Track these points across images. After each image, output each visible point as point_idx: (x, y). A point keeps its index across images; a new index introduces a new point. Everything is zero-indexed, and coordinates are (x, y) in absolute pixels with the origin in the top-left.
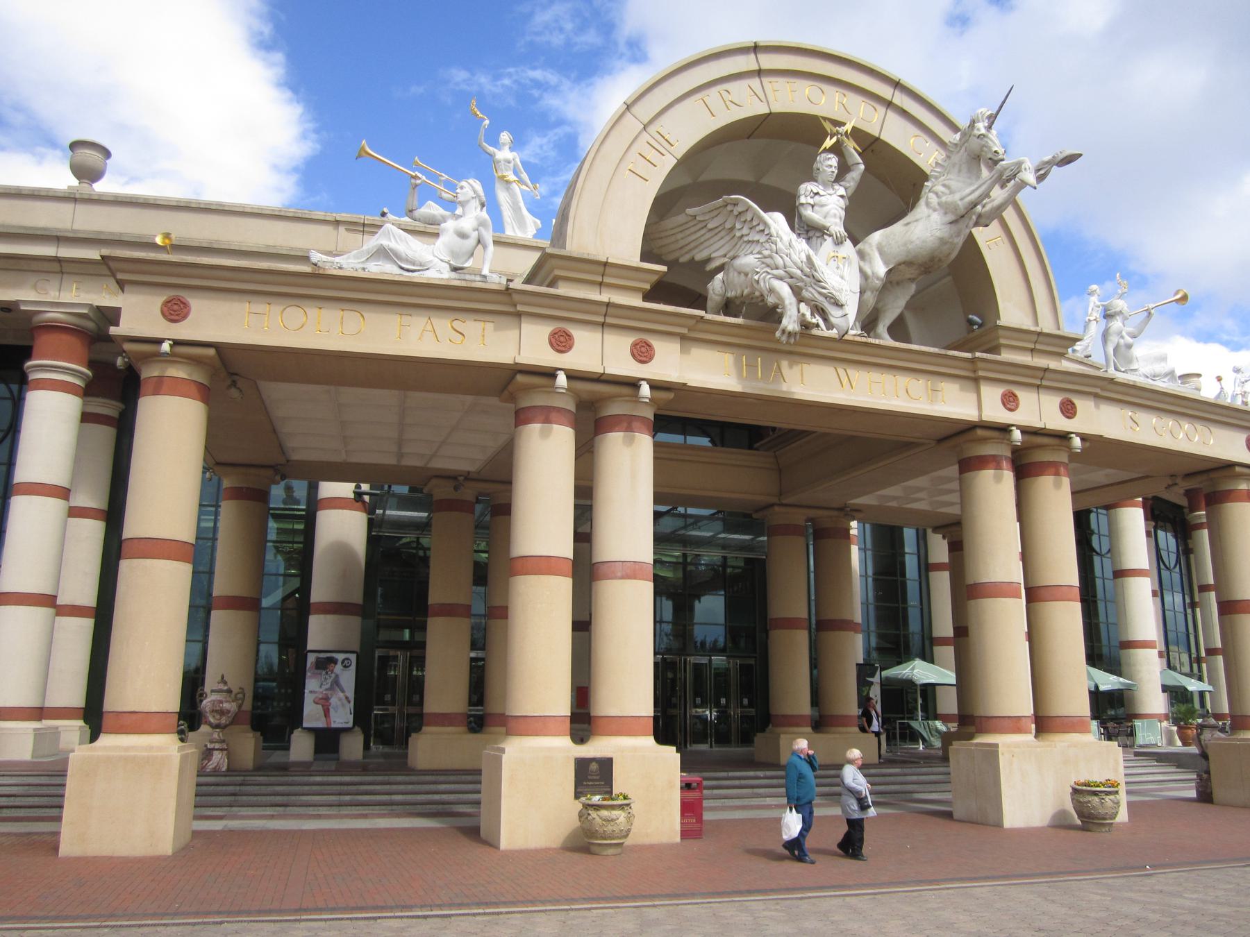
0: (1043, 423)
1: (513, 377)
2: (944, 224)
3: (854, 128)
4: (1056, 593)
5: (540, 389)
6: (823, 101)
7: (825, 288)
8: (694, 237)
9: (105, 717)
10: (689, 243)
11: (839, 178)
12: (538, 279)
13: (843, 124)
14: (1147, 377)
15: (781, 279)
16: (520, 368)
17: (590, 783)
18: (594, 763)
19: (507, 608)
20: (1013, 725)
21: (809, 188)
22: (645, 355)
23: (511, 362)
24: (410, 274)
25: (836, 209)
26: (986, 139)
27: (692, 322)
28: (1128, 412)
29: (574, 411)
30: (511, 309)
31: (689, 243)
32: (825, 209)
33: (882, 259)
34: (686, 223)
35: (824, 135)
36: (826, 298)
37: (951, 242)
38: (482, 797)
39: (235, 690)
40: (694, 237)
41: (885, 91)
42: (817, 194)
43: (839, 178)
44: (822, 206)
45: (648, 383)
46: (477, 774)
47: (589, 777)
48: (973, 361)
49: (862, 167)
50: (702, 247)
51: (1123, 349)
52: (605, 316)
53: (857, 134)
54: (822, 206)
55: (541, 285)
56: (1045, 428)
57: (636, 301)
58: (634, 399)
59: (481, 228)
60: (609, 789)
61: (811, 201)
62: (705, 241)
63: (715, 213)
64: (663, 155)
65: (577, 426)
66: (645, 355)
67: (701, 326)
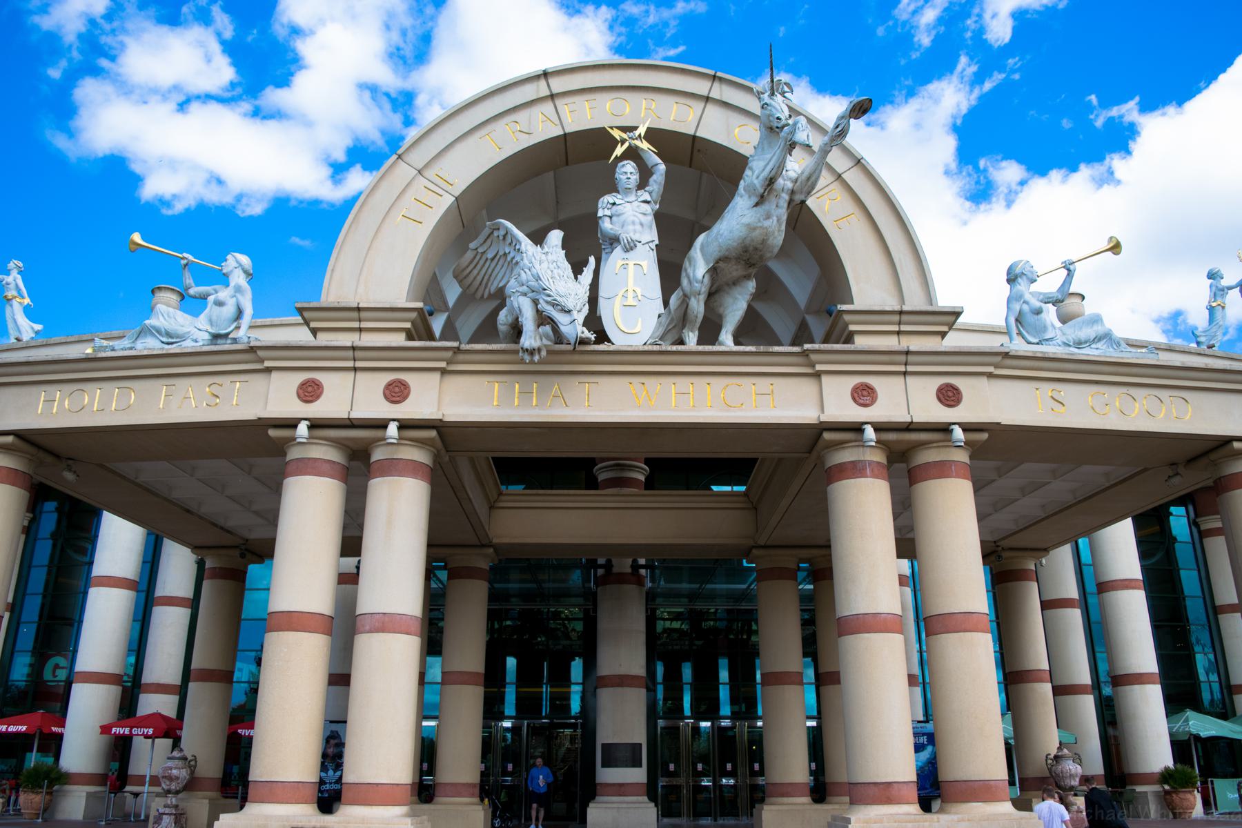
0: (441, 413)
1: (821, 434)
2: (748, 209)
3: (649, 130)
4: (960, 623)
5: (847, 445)
6: (628, 111)
7: (549, 296)
10: (483, 278)
11: (642, 185)
12: (834, 337)
13: (636, 128)
14: (1069, 346)
15: (525, 294)
19: (838, 673)
20: (884, 793)
21: (606, 201)
22: (953, 398)
23: (814, 421)
24: (170, 346)
25: (634, 216)
26: (769, 108)
27: (449, 354)
28: (1047, 388)
29: (968, 463)
30: (809, 370)
31: (483, 278)
32: (622, 218)
33: (704, 259)
34: (475, 257)
35: (614, 143)
36: (553, 306)
37: (761, 227)
39: (190, 758)
42: (614, 204)
43: (642, 185)
44: (618, 215)
45: (872, 427)
49: (662, 167)
50: (492, 279)
51: (1030, 318)
53: (653, 135)
54: (618, 215)
55: (837, 343)
56: (912, 422)
57: (399, 340)
58: (861, 443)
59: (238, 295)
61: (608, 213)
62: (492, 272)
63: (489, 241)
64: (441, 196)
65: (891, 478)
66: (953, 398)
67: (461, 357)
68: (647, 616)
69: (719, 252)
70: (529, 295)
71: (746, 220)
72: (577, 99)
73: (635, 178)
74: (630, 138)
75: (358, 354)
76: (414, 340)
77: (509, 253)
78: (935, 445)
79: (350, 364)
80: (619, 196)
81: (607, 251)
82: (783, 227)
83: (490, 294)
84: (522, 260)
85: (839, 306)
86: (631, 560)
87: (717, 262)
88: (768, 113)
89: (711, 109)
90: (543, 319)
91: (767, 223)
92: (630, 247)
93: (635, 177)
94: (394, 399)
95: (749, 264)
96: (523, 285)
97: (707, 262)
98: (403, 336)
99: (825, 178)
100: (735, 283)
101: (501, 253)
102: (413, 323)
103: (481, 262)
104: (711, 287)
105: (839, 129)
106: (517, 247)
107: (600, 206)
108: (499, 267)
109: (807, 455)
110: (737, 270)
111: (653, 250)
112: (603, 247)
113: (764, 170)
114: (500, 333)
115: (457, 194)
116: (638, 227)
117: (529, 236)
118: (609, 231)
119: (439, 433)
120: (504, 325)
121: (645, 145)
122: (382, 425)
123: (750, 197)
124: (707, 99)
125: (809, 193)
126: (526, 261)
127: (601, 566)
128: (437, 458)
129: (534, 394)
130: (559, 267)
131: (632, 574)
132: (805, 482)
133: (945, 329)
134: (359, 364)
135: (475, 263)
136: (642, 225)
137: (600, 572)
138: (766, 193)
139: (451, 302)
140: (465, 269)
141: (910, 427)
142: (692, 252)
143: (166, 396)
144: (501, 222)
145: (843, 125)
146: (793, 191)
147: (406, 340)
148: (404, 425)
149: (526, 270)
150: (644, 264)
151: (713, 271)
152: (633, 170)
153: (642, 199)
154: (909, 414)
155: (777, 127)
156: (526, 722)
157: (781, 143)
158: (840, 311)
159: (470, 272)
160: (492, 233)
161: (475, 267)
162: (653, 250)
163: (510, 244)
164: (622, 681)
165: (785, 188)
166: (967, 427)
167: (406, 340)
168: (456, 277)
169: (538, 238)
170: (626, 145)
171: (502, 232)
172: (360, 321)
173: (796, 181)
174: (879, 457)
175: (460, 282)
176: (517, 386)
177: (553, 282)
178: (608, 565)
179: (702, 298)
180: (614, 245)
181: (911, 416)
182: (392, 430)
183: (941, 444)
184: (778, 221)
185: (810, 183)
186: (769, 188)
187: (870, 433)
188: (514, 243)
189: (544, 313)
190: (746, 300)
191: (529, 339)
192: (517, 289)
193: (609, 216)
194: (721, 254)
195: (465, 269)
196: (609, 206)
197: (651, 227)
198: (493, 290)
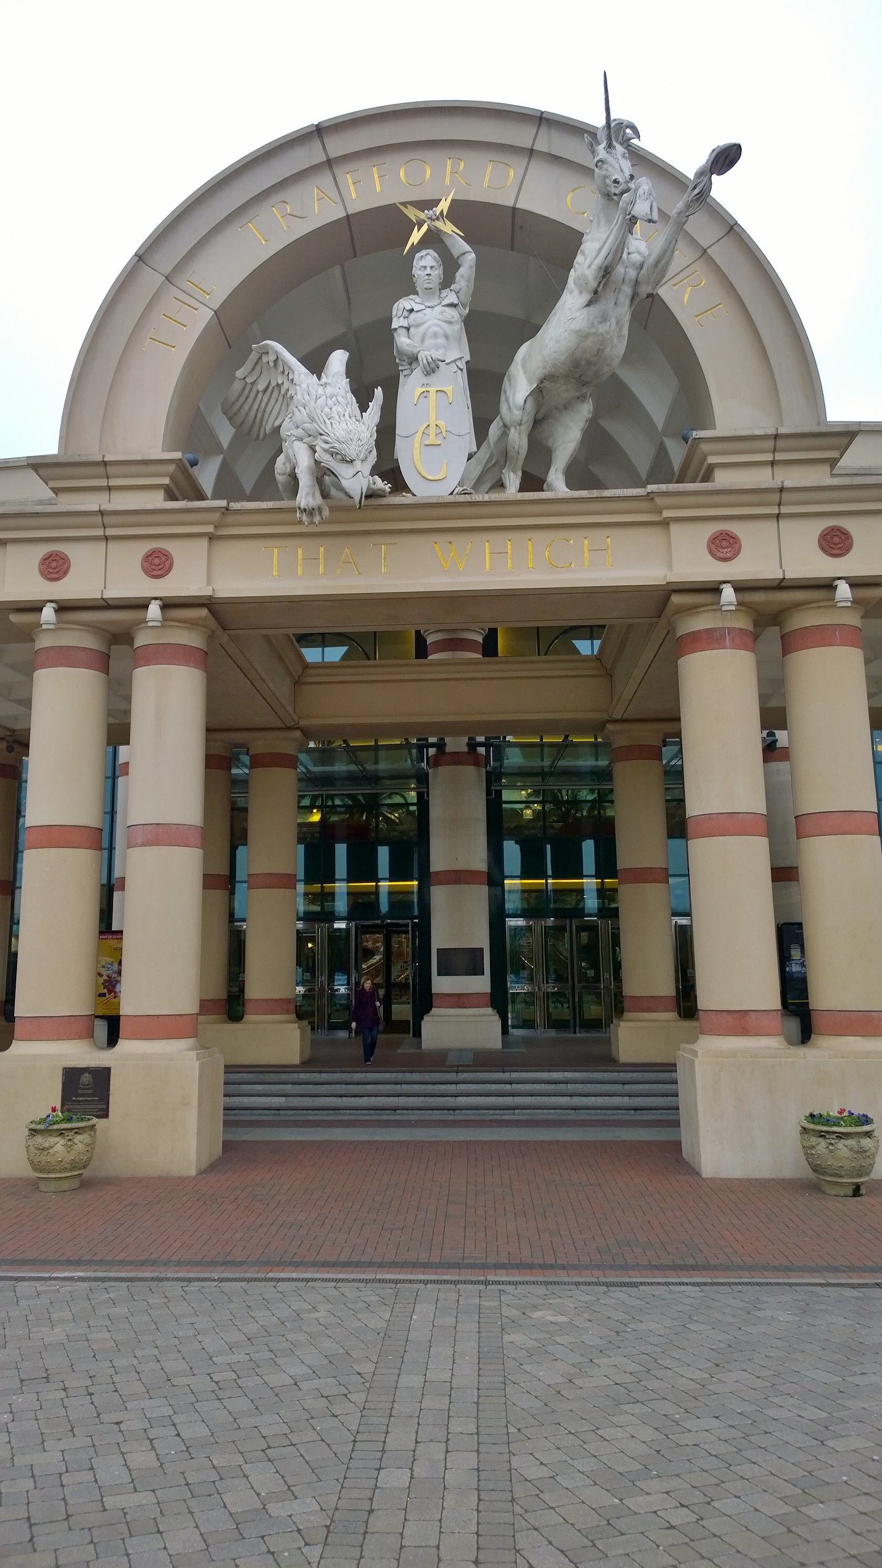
1: (667, 599)
5: (809, 606)
7: (327, 443)
8: (256, 406)
9: (434, 998)
10: (256, 415)
11: (447, 281)
13: (436, 202)
15: (300, 439)
16: (674, 588)
17: (81, 1099)
18: (86, 1074)
21: (401, 306)
22: (839, 546)
26: (605, 166)
27: (216, 516)
31: (256, 415)
32: (422, 329)
34: (244, 389)
35: (410, 226)
37: (595, 333)
38: (682, 1101)
40: (256, 406)
41: (522, 136)
42: (412, 311)
44: (418, 326)
46: (671, 1071)
47: (80, 1091)
48: (650, 497)
49: (471, 257)
52: (779, 505)
57: (157, 500)
60: (104, 1107)
64: (196, 309)
66: (839, 546)
67: (230, 519)
68: (488, 801)
69: (544, 368)
70: (306, 440)
71: (576, 325)
72: (362, 166)
73: (438, 273)
74: (429, 218)
75: (107, 520)
76: (177, 500)
77: (283, 383)
78: (814, 605)
79: (99, 532)
80: (418, 300)
81: (405, 373)
82: (625, 331)
83: (265, 434)
84: (296, 394)
85: (694, 433)
86: (467, 739)
87: (542, 382)
88: (604, 173)
89: (538, 170)
90: (322, 474)
91: (602, 328)
92: (431, 369)
93: (437, 272)
94: (155, 573)
95: (583, 383)
96: (298, 427)
97: (530, 381)
98: (161, 494)
99: (682, 257)
100: (567, 406)
101: (273, 384)
102: (172, 478)
103: (252, 395)
104: (537, 412)
105: (697, 191)
106: (290, 377)
107: (394, 313)
108: (273, 401)
109: (656, 620)
110: (567, 391)
111: (462, 370)
112: (400, 368)
113: (598, 255)
114: (279, 485)
115: (216, 307)
116: (441, 341)
117: (304, 361)
118: (406, 348)
119: (210, 610)
120: (283, 474)
121: (448, 228)
122: (142, 605)
123: (581, 293)
124: (531, 153)
125: (657, 283)
126: (299, 396)
127: (433, 745)
128: (211, 637)
129: (321, 561)
130: (339, 403)
131: (468, 753)
132: (658, 650)
133: (834, 454)
134: (110, 532)
135: (245, 395)
136: (446, 337)
137: (432, 751)
138: (601, 287)
139: (225, 444)
140: (234, 403)
141: (783, 584)
142: (512, 368)
143: (318, 200)
144: (268, 345)
145: (702, 185)
146: (637, 281)
147: (165, 500)
148: (168, 605)
149: (300, 408)
150: (449, 389)
151: (538, 393)
152: (433, 263)
153: (447, 301)
154: (781, 568)
155: (615, 194)
156: (354, 923)
157: (618, 217)
158: (695, 439)
159: (241, 407)
160: (260, 358)
161: (245, 401)
162: (462, 370)
163: (283, 372)
164: (458, 877)
165: (627, 277)
166: (855, 582)
167: (165, 500)
168: (225, 413)
169: (316, 365)
170: (425, 228)
171: (272, 358)
172: (108, 478)
173: (641, 266)
174: (743, 623)
175: (231, 419)
176: (300, 552)
177: (331, 423)
178: (440, 746)
179: (525, 429)
180: (414, 366)
181: (784, 571)
182: (154, 610)
183: (822, 604)
184: (617, 323)
185: (659, 268)
186: (605, 280)
187: (728, 594)
188: (286, 371)
189: (322, 464)
190: (580, 428)
191: (307, 496)
192: (292, 432)
193: (405, 328)
194: (546, 371)
195: (234, 403)
196: (405, 313)
197: (459, 340)
198: (268, 428)
